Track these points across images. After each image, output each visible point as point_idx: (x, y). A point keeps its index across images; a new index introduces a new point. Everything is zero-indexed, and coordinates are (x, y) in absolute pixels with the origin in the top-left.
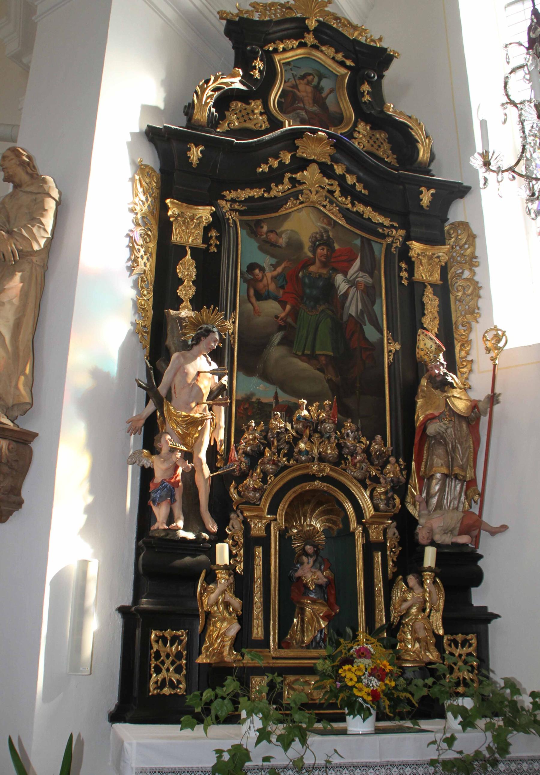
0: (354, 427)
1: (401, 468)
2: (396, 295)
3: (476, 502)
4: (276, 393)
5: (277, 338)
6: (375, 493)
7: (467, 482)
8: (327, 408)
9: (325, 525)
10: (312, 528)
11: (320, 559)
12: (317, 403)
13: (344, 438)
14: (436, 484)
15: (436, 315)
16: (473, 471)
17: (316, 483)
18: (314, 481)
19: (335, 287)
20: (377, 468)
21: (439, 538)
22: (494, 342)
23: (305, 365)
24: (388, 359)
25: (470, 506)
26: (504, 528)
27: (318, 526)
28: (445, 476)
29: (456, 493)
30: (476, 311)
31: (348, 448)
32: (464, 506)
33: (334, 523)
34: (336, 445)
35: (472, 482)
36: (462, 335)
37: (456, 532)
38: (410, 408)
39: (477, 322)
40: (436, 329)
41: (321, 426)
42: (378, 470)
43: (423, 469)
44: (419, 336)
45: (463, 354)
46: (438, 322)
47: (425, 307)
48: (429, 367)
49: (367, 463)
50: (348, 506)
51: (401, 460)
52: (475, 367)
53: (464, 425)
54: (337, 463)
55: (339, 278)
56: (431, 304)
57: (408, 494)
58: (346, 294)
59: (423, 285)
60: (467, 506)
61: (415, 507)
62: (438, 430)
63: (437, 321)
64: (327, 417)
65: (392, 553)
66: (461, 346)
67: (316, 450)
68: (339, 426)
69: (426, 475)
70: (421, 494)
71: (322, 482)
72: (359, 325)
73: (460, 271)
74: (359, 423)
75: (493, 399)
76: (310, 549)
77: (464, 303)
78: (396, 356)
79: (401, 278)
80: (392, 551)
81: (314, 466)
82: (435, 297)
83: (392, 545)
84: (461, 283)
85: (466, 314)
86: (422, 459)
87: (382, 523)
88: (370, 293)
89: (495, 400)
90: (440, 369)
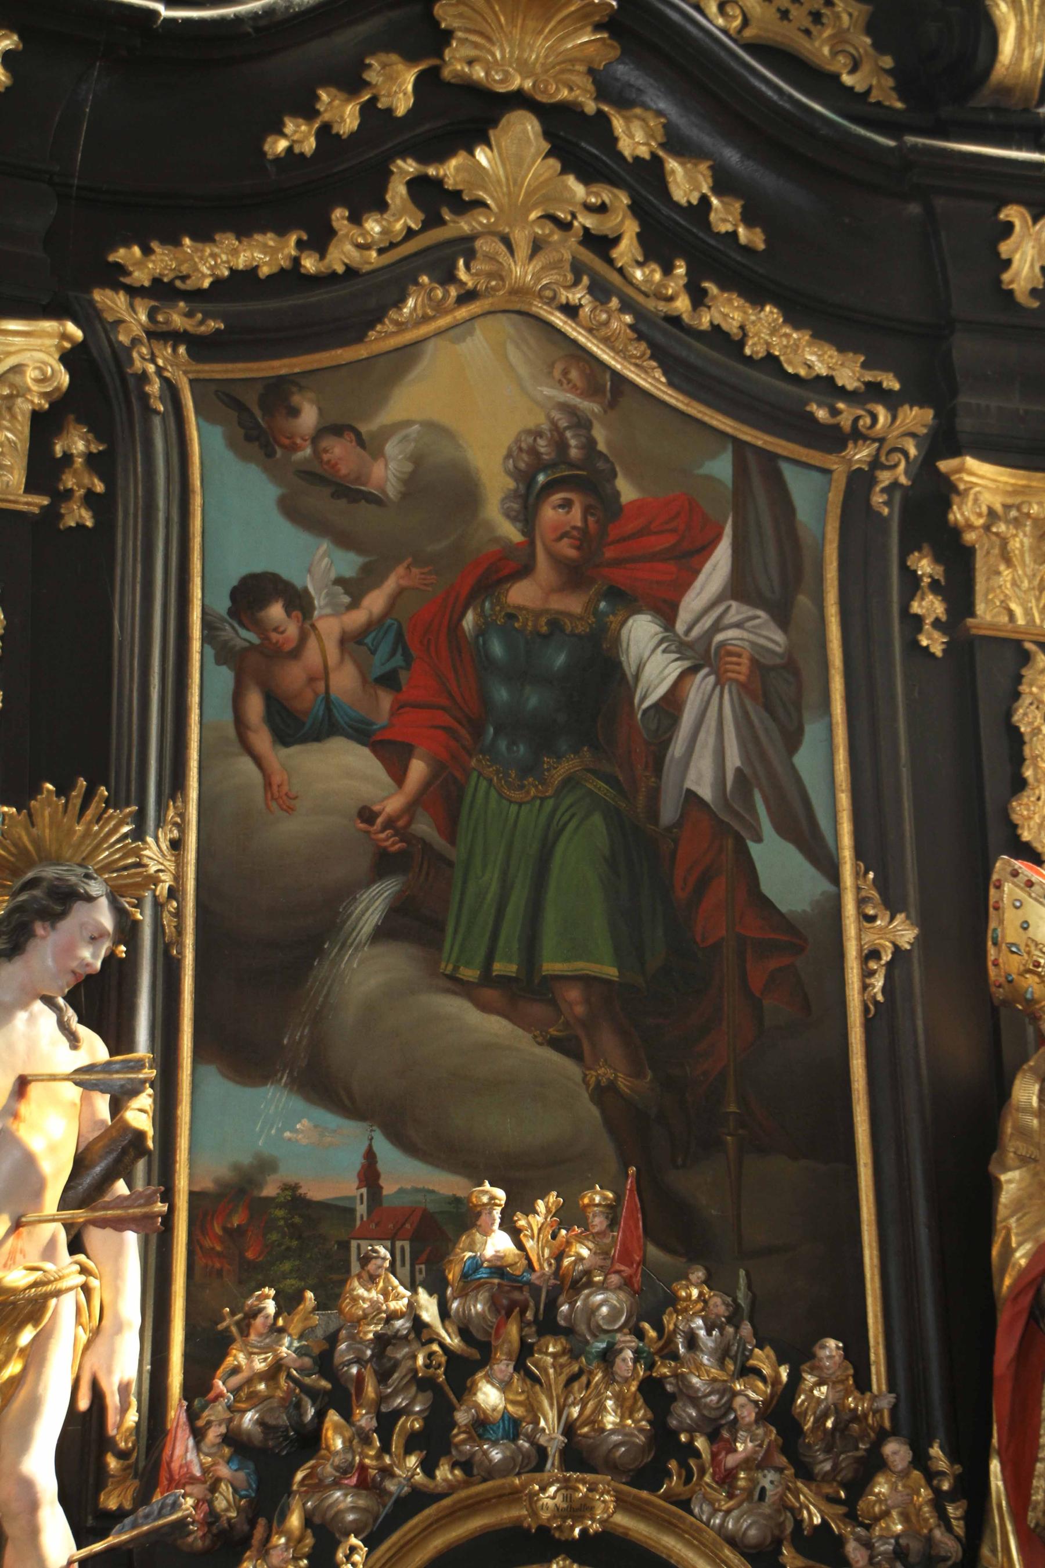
0: (719, 1305)
1: (937, 1491)
4: (370, 1156)
5: (372, 907)
8: (599, 1223)
12: (552, 1197)
13: (675, 1356)
19: (624, 675)
20: (827, 1490)
23: (495, 1026)
24: (865, 987)
31: (694, 1400)
34: (640, 1388)
41: (572, 1304)
42: (834, 1500)
44: (999, 887)
47: (1027, 751)
49: (780, 1470)
51: (935, 1451)
55: (641, 632)
58: (671, 705)
64: (598, 1261)
67: (552, 1414)
68: (652, 1303)
72: (730, 843)
74: (742, 1281)
78: (897, 972)
79: (917, 621)
81: (543, 1489)
88: (776, 697)
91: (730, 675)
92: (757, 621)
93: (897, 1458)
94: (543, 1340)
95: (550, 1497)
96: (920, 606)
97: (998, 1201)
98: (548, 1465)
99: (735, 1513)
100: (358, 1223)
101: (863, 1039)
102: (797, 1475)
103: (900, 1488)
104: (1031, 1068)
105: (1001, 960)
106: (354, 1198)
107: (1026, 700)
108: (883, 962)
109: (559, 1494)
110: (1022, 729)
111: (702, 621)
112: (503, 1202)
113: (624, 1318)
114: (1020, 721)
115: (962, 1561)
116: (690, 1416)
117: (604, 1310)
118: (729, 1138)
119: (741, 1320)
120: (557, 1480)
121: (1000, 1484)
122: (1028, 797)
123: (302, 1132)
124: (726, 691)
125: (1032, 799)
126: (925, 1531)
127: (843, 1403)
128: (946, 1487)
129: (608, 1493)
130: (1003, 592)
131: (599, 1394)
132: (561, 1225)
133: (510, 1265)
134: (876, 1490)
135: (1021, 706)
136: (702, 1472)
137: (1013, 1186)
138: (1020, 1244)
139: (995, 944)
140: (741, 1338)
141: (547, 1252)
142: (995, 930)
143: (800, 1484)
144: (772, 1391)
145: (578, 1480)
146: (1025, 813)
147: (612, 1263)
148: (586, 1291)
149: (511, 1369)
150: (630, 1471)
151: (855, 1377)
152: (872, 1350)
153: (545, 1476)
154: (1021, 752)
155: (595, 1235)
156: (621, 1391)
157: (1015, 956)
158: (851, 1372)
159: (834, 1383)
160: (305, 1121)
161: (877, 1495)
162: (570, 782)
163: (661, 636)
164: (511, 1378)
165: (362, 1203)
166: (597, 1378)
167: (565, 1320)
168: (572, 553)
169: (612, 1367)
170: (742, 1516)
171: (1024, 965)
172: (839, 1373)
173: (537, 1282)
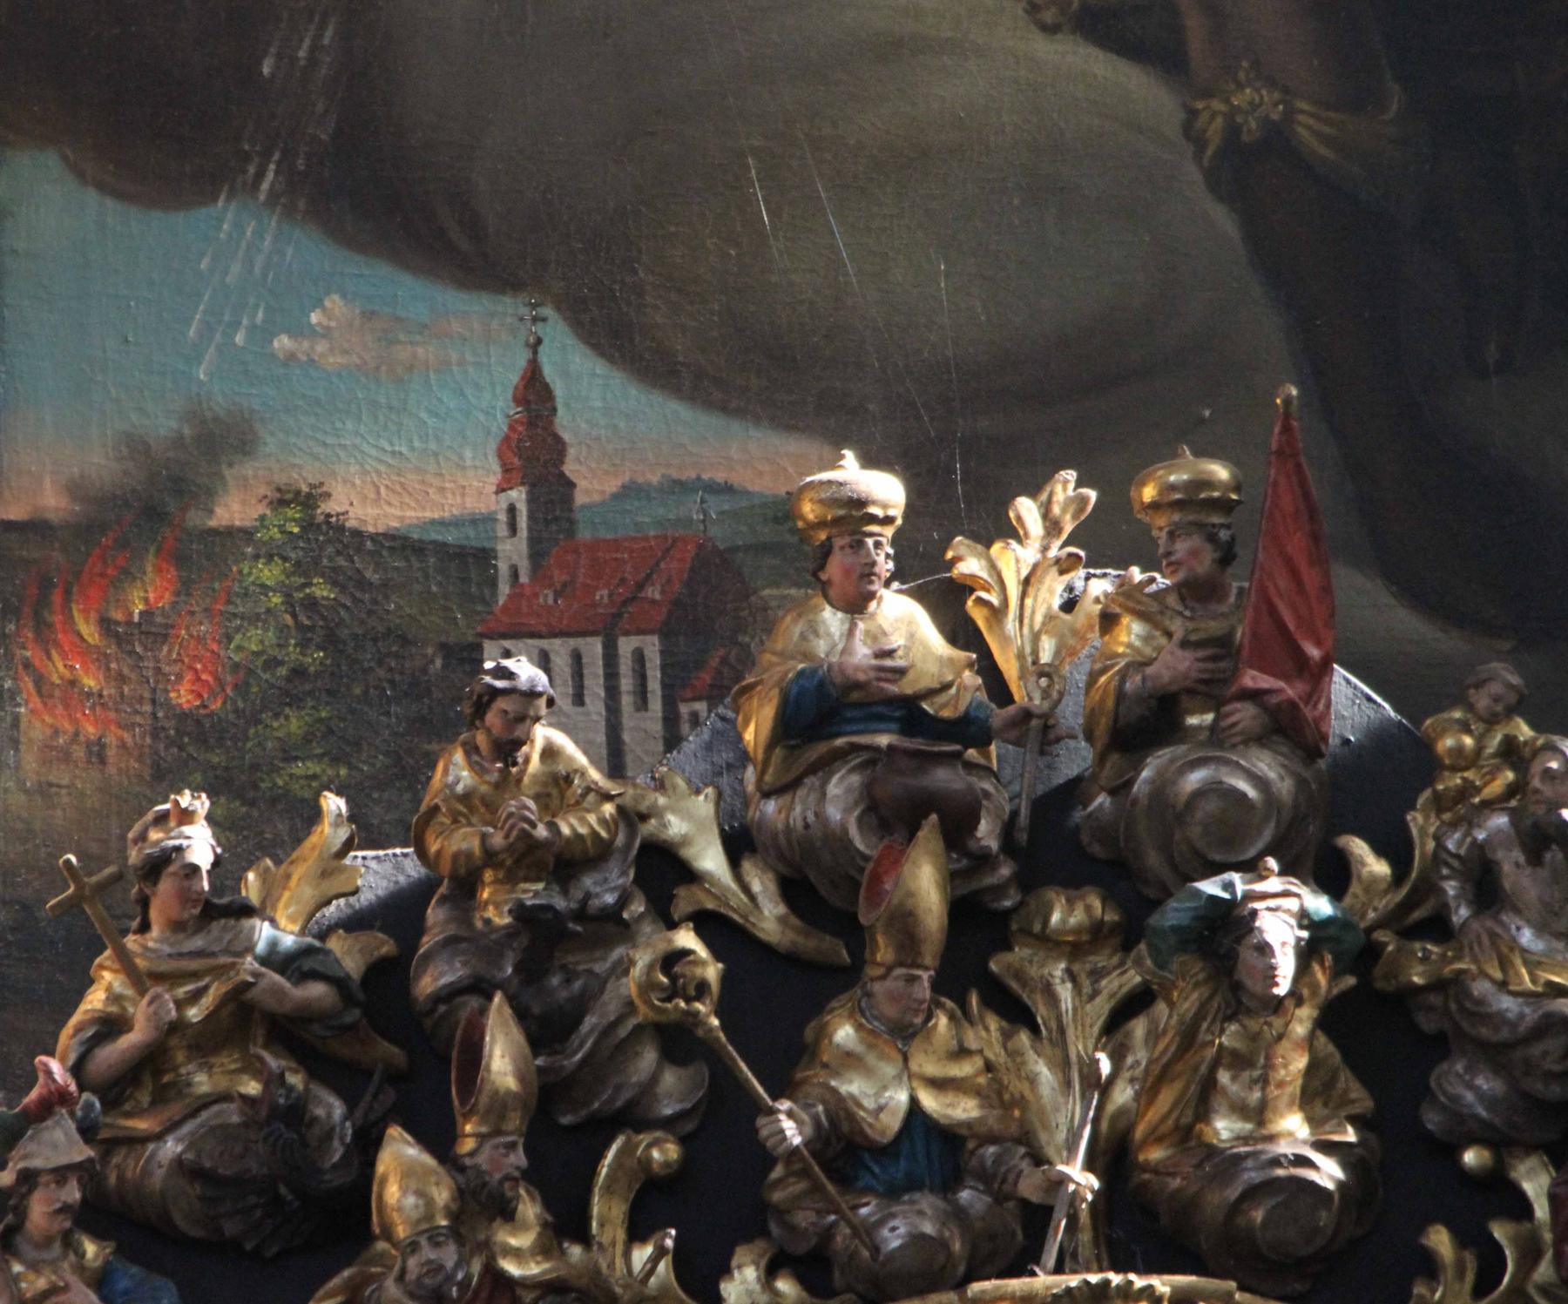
4: (534, 394)
12: (1065, 485)
13: (1439, 928)
100: (504, 589)
106: (490, 519)
112: (897, 512)
123: (327, 333)
133: (931, 693)
136: (1530, 1253)
160: (334, 302)
165: (513, 528)
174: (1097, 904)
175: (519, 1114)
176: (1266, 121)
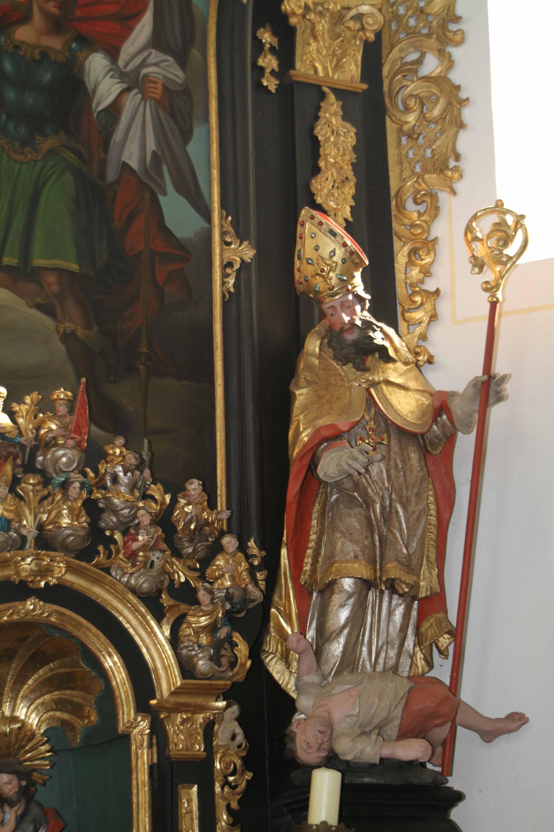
0: (131, 459)
1: (251, 565)
2: (245, 115)
3: (443, 653)
6: (186, 631)
7: (421, 600)
8: (62, 410)
9: (51, 718)
10: (17, 726)
11: (35, 810)
12: (35, 395)
13: (105, 488)
14: (342, 606)
15: (350, 173)
16: (435, 572)
17: (29, 605)
18: (23, 598)
19: (86, 90)
20: (189, 563)
21: (347, 748)
22: (492, 243)
24: (223, 283)
25: (430, 664)
26: (516, 721)
27: (34, 720)
28: (365, 585)
29: (391, 629)
30: (452, 163)
31: (115, 512)
32: (413, 664)
33: (76, 709)
34: (83, 505)
35: (434, 602)
36: (413, 226)
37: (393, 730)
38: (276, 410)
39: (454, 192)
40: (348, 209)
41: (45, 455)
42: (194, 569)
43: (307, 568)
44: (303, 225)
45: (415, 273)
46: (353, 191)
47: (321, 150)
48: (325, 307)
49: (163, 551)
50: (113, 663)
51: (252, 543)
52: (444, 307)
53: (414, 456)
54: (86, 553)
55: (96, 64)
56: (335, 144)
57: (268, 632)
58: (114, 110)
59: (317, 93)
60: (420, 663)
61: (288, 665)
62: (346, 467)
63: (349, 190)
64: (62, 432)
65: (226, 789)
66: (409, 255)
67: (31, 518)
68: (93, 456)
69: (316, 581)
70: (303, 632)
71: (45, 601)
72: (148, 195)
73: (414, 56)
74: (146, 446)
75: (488, 388)
76: (9, 782)
77: (421, 141)
78: (242, 275)
79: (261, 71)
80: (226, 783)
81: (23, 560)
82: (348, 125)
83: (227, 768)
84: (416, 88)
85: (425, 170)
86: (307, 541)
87: (201, 709)
88: (177, 110)
89: (491, 392)
90: (354, 313)
91: (150, 94)
92: (168, 63)
93: (230, 545)
94: (27, 476)
95: (28, 564)
96: (263, 61)
97: (293, 406)
98: (27, 546)
99: (135, 575)
101: (221, 313)
102: (172, 555)
103: (231, 562)
104: (316, 331)
105: (302, 269)
107: (322, 121)
108: (235, 269)
109: (33, 562)
110: (320, 138)
111: (135, 60)
112: (5, 396)
113: (75, 465)
114: (318, 133)
115: (263, 602)
116: (113, 522)
117: (64, 459)
118: (141, 367)
119: (145, 467)
120: (32, 555)
121: (287, 561)
122: (321, 178)
124: (148, 104)
125: (323, 179)
126: (243, 586)
127: (201, 516)
128: (256, 563)
129: (62, 562)
130: (311, 56)
131: (59, 507)
132: (40, 411)
133: (9, 433)
134: (218, 563)
135: (319, 124)
136: (118, 552)
137: (302, 397)
138: (304, 430)
139: (299, 258)
140: (144, 477)
141: (31, 426)
142: (299, 250)
143: (174, 560)
144: (160, 509)
145: (44, 555)
146: (319, 187)
147: (70, 433)
148: (54, 449)
149: (7, 491)
150: (75, 551)
151: (208, 501)
152: (219, 488)
153: (25, 552)
154: (318, 151)
155: (60, 417)
156: (72, 506)
157: (310, 266)
158: (206, 498)
159: (196, 504)
161: (217, 566)
162: (52, 152)
163: (109, 68)
164: (7, 496)
166: (58, 498)
167: (41, 465)
168: (55, 11)
169: (67, 492)
170: (139, 577)
171: (315, 271)
172: (199, 499)
173: (24, 443)
174: (40, 478)
175: (178, 506)
176: (71, 330)
